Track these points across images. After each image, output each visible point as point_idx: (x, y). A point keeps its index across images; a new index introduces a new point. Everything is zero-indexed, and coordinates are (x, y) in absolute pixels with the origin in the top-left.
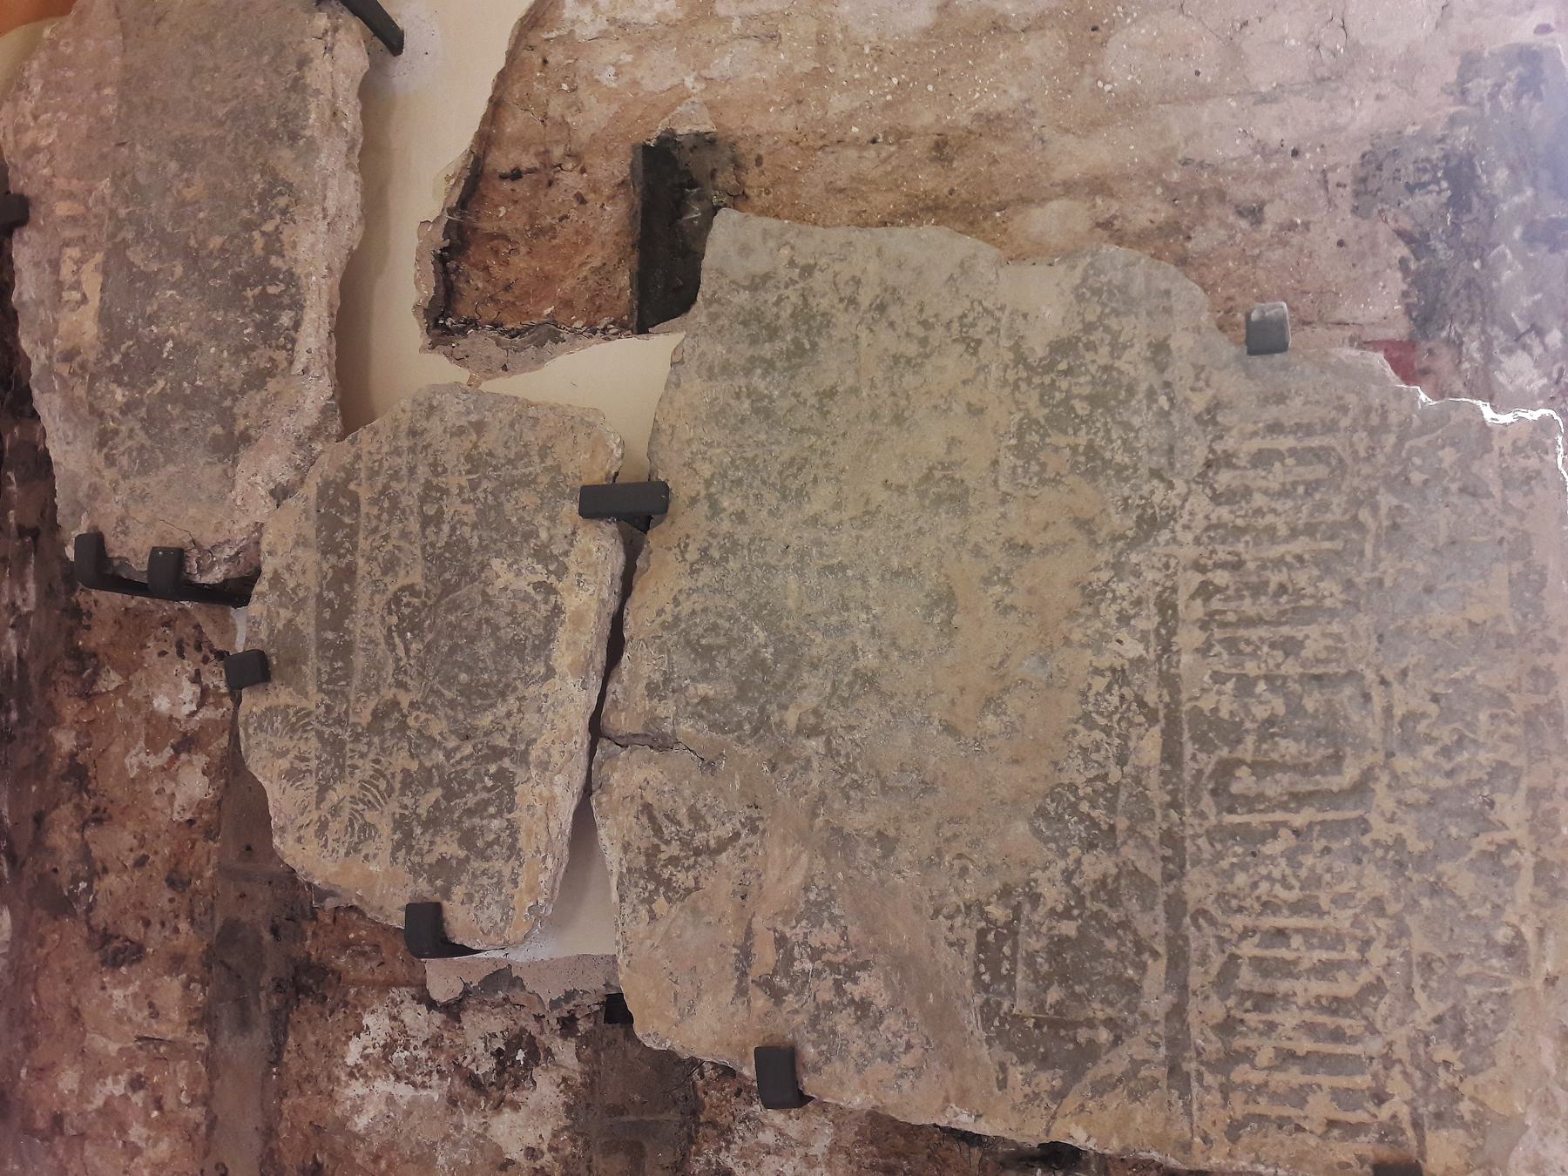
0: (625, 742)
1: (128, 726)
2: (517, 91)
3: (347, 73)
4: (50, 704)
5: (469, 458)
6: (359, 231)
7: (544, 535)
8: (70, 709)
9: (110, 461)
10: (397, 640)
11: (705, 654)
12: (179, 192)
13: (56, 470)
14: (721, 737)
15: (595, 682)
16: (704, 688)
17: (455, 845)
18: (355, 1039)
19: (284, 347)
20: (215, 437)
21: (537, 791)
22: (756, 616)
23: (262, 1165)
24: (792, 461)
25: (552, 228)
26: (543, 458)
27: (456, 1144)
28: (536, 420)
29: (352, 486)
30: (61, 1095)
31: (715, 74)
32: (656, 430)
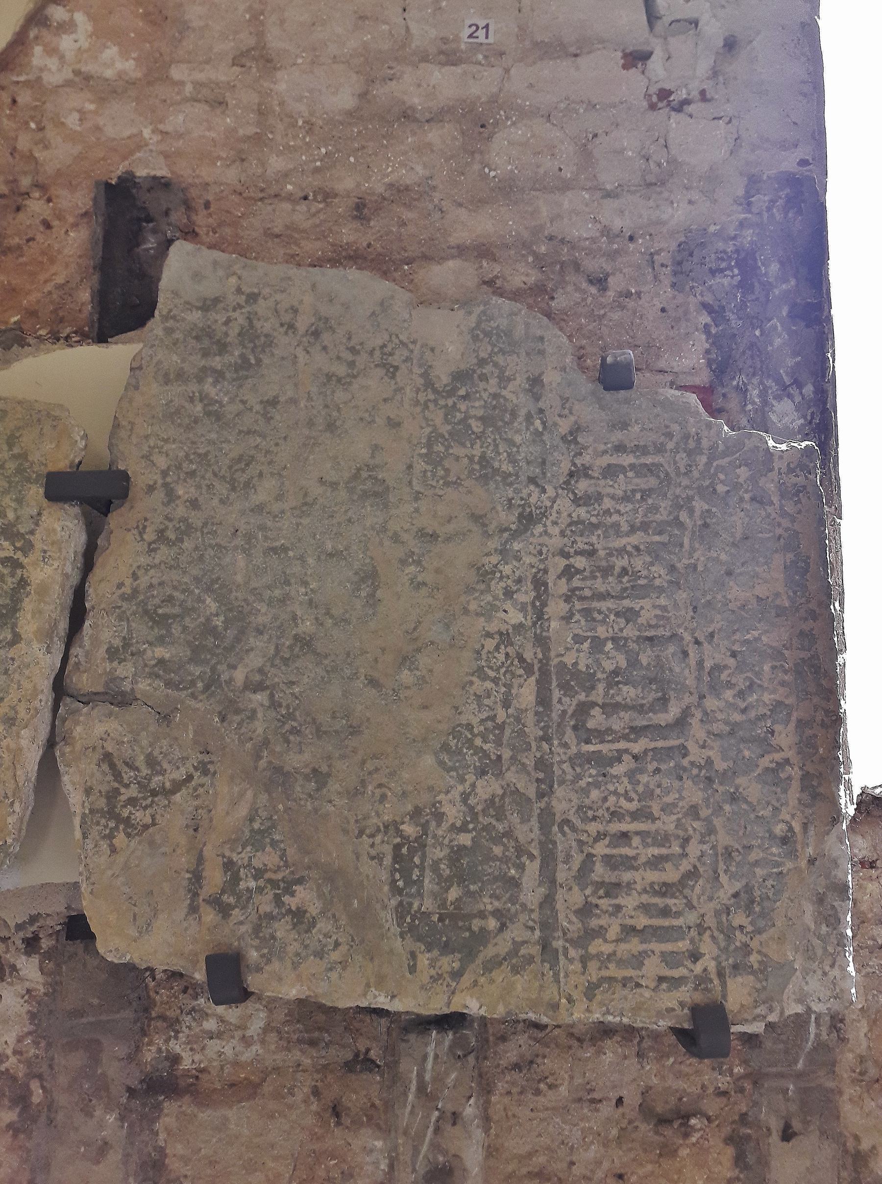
0: (87, 699)
7: (11, 515)
11: (160, 621)
15: (59, 647)
16: (160, 652)
22: (209, 589)
24: (240, 459)
25: (19, 247)
31: (169, 128)
32: (116, 426)
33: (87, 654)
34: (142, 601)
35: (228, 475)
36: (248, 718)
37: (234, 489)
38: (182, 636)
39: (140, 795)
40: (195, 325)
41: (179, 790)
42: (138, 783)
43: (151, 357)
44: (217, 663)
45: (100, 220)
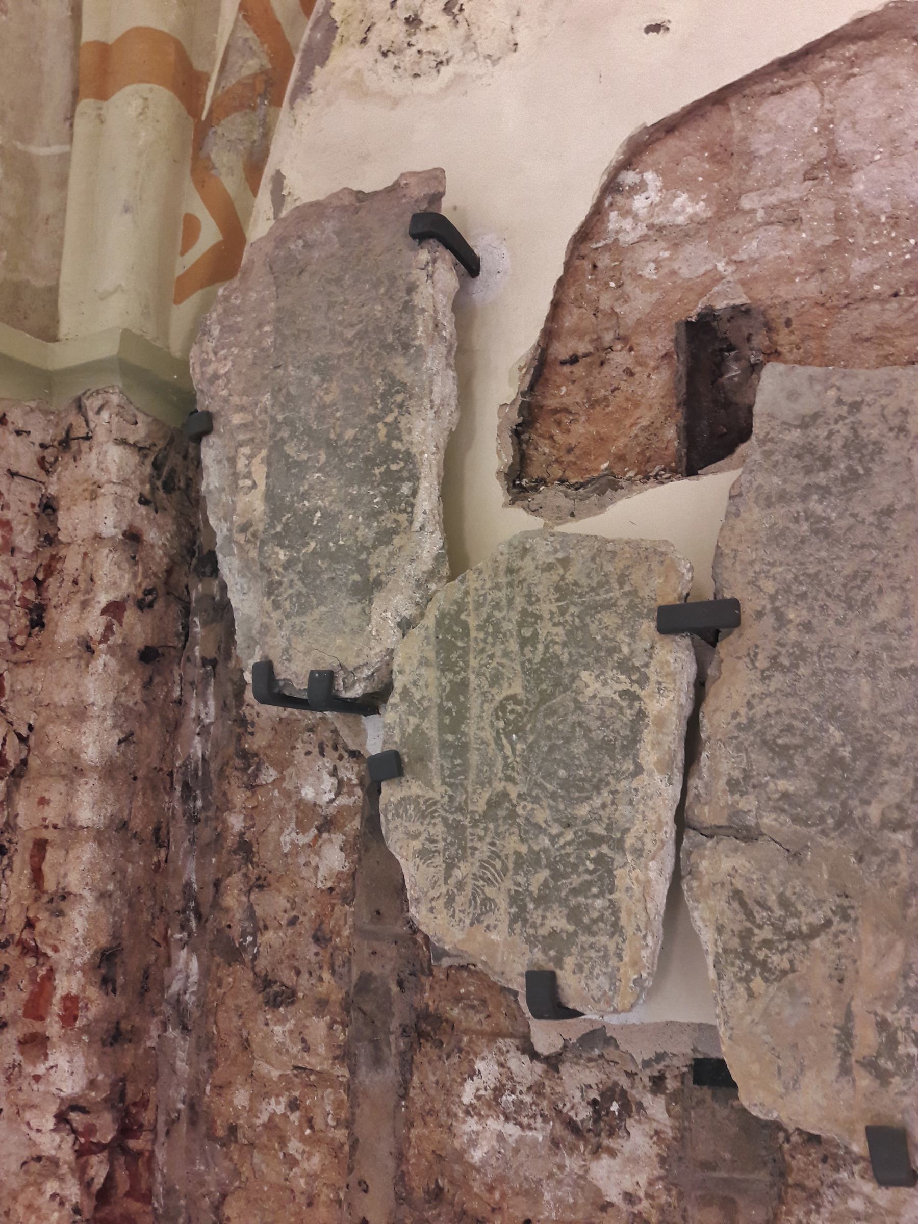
0: (711, 833)
1: (282, 811)
2: (572, 293)
3: (444, 294)
4: (225, 794)
5: (558, 589)
6: (456, 416)
7: (626, 650)
8: (239, 797)
9: (277, 605)
10: (505, 741)
11: (783, 752)
12: (321, 398)
13: (236, 615)
14: (802, 830)
15: (678, 777)
16: (784, 785)
17: (564, 921)
18: (469, 1081)
19: (405, 511)
20: (355, 583)
21: (633, 874)
22: (831, 717)
23: (395, 1184)
24: (855, 576)
25: (606, 398)
26: (621, 584)
27: (560, 1182)
28: (614, 553)
29: (463, 617)
30: (235, 1109)
31: (744, 257)
32: (719, 554)
33: (707, 786)
34: (759, 731)
35: (843, 594)
36: (890, 860)
37: (850, 608)
38: (806, 768)
39: (776, 938)
40: (794, 443)
41: (818, 936)
42: (772, 924)
43: (751, 482)
44: (847, 798)
45: (682, 359)
